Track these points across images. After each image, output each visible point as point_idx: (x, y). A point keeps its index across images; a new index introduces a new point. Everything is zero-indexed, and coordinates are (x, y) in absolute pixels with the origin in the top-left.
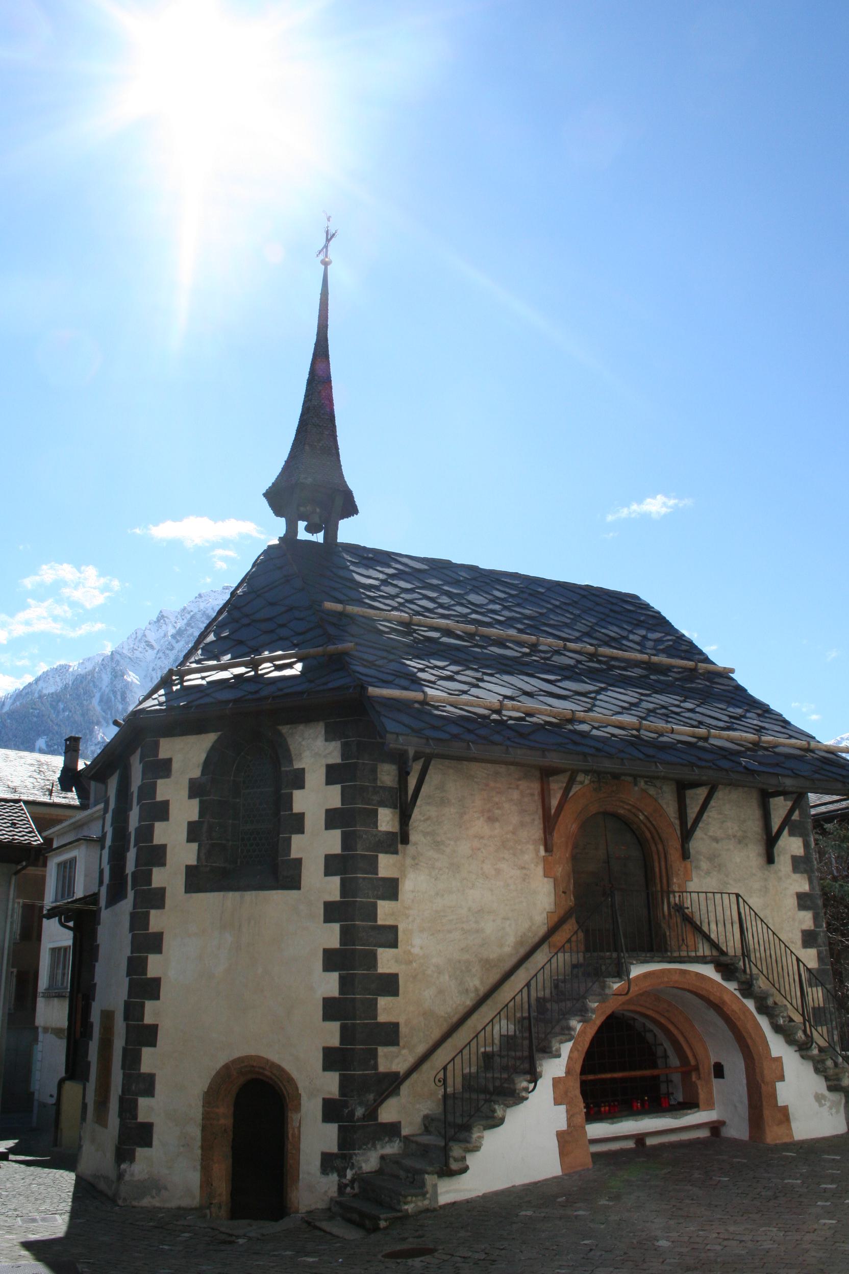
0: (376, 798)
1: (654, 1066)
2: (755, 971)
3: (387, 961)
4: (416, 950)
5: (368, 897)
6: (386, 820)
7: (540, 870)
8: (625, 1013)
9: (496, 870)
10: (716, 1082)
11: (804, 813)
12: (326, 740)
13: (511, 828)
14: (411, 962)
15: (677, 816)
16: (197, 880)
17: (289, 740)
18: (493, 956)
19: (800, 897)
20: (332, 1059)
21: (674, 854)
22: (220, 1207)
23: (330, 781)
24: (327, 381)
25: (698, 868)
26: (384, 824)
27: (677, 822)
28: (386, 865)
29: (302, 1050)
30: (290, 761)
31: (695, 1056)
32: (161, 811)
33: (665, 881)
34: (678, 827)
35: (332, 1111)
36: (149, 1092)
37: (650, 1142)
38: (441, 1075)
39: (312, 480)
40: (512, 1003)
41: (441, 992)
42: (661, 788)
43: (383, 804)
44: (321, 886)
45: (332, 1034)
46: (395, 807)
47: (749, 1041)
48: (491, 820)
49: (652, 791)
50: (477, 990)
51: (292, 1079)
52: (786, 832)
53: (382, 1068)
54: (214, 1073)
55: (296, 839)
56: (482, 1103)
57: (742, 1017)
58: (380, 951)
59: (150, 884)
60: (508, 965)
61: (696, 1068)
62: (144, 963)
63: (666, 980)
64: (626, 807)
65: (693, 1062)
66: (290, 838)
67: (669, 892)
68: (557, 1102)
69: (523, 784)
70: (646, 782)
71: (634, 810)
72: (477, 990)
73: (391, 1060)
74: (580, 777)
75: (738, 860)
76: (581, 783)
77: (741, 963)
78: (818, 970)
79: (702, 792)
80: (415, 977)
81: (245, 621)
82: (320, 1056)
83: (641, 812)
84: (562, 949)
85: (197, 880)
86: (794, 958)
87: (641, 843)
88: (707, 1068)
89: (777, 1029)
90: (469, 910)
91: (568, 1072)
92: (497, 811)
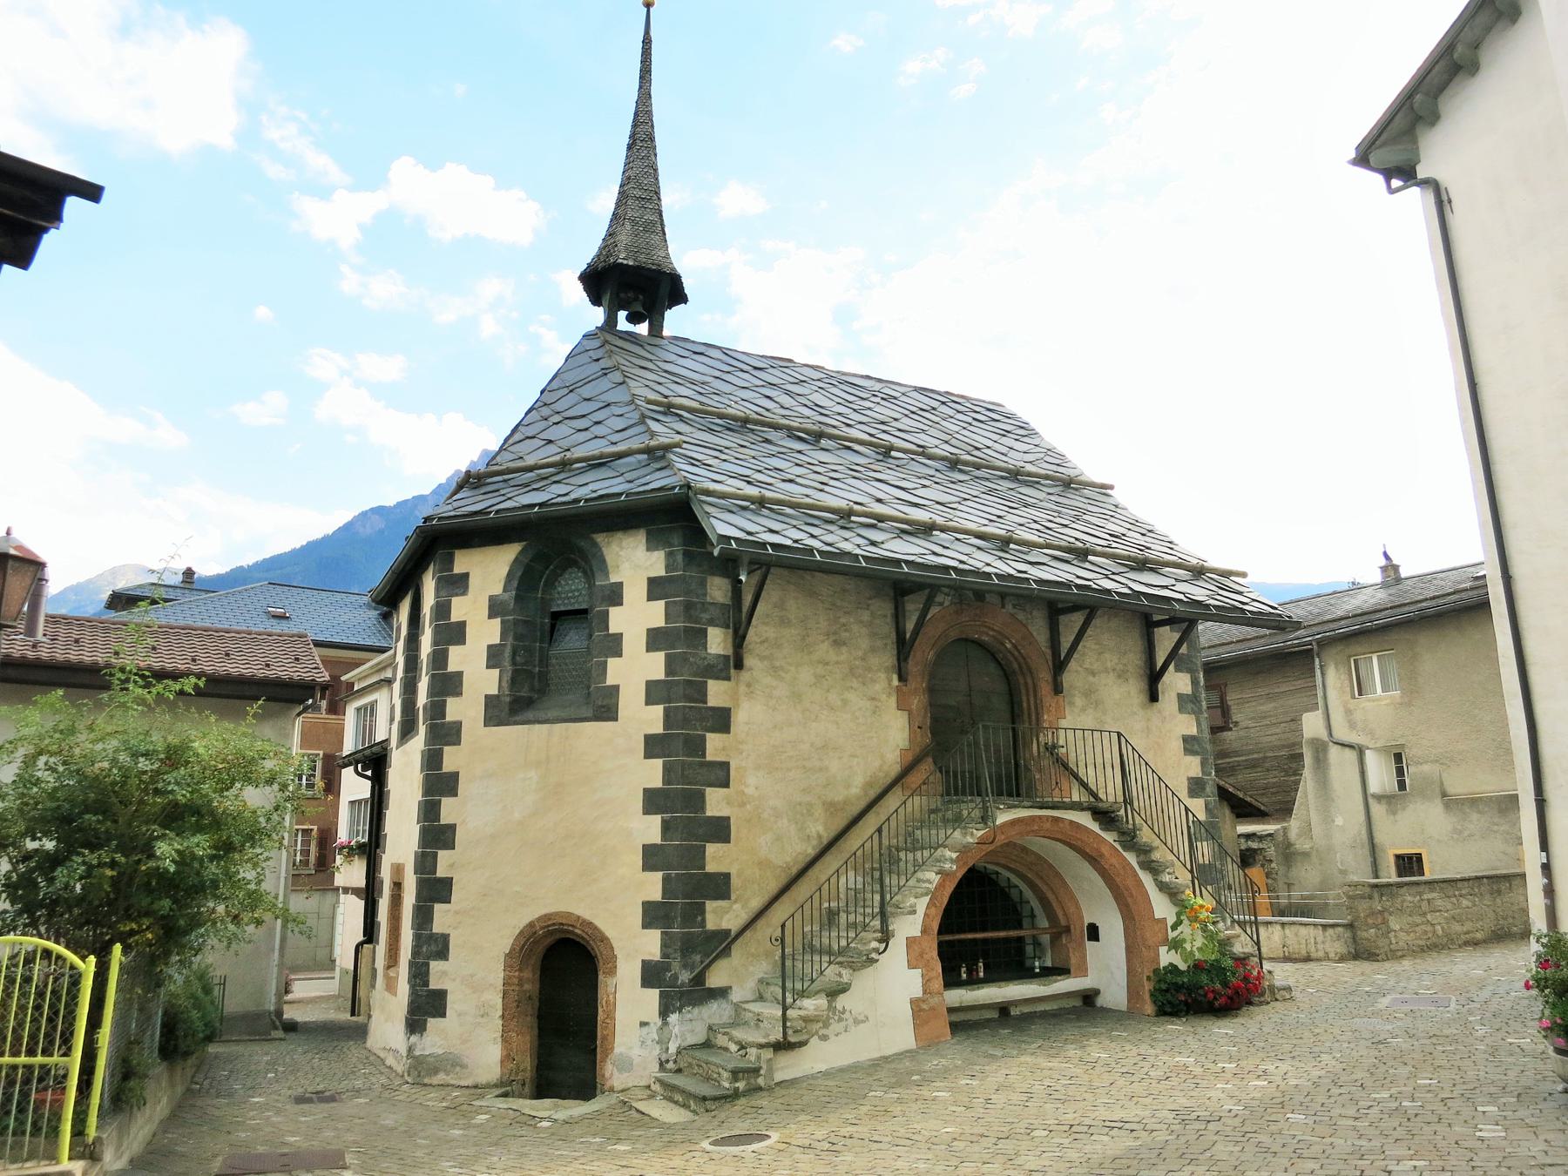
0: (705, 616)
1: (1019, 926)
2: (1138, 820)
3: (716, 803)
4: (750, 791)
6: (717, 642)
7: (893, 701)
8: (990, 867)
10: (1090, 945)
11: (1194, 646)
13: (860, 653)
16: (501, 711)
17: (605, 551)
18: (839, 798)
19: (1187, 740)
20: (653, 915)
21: (1045, 688)
23: (652, 596)
24: (649, 113)
25: (1072, 704)
27: (1049, 651)
28: (717, 693)
31: (1065, 914)
32: (452, 634)
34: (1049, 657)
35: (651, 975)
36: (443, 954)
38: (778, 933)
39: (633, 283)
40: (859, 853)
41: (778, 838)
43: (712, 623)
45: (652, 886)
46: (727, 627)
48: (838, 643)
49: (1021, 616)
50: (820, 837)
52: (1171, 667)
55: (612, 663)
56: (825, 965)
58: (709, 790)
59: (444, 717)
61: (1068, 930)
65: (1063, 923)
67: (1038, 727)
68: (911, 966)
70: (1014, 606)
72: (820, 837)
74: (939, 598)
75: (1117, 696)
76: (941, 604)
77: (1122, 812)
79: (1077, 619)
80: (749, 821)
81: (557, 418)
84: (916, 791)
85: (501, 711)
87: (1008, 676)
89: (1163, 887)
90: (812, 745)
91: (924, 931)
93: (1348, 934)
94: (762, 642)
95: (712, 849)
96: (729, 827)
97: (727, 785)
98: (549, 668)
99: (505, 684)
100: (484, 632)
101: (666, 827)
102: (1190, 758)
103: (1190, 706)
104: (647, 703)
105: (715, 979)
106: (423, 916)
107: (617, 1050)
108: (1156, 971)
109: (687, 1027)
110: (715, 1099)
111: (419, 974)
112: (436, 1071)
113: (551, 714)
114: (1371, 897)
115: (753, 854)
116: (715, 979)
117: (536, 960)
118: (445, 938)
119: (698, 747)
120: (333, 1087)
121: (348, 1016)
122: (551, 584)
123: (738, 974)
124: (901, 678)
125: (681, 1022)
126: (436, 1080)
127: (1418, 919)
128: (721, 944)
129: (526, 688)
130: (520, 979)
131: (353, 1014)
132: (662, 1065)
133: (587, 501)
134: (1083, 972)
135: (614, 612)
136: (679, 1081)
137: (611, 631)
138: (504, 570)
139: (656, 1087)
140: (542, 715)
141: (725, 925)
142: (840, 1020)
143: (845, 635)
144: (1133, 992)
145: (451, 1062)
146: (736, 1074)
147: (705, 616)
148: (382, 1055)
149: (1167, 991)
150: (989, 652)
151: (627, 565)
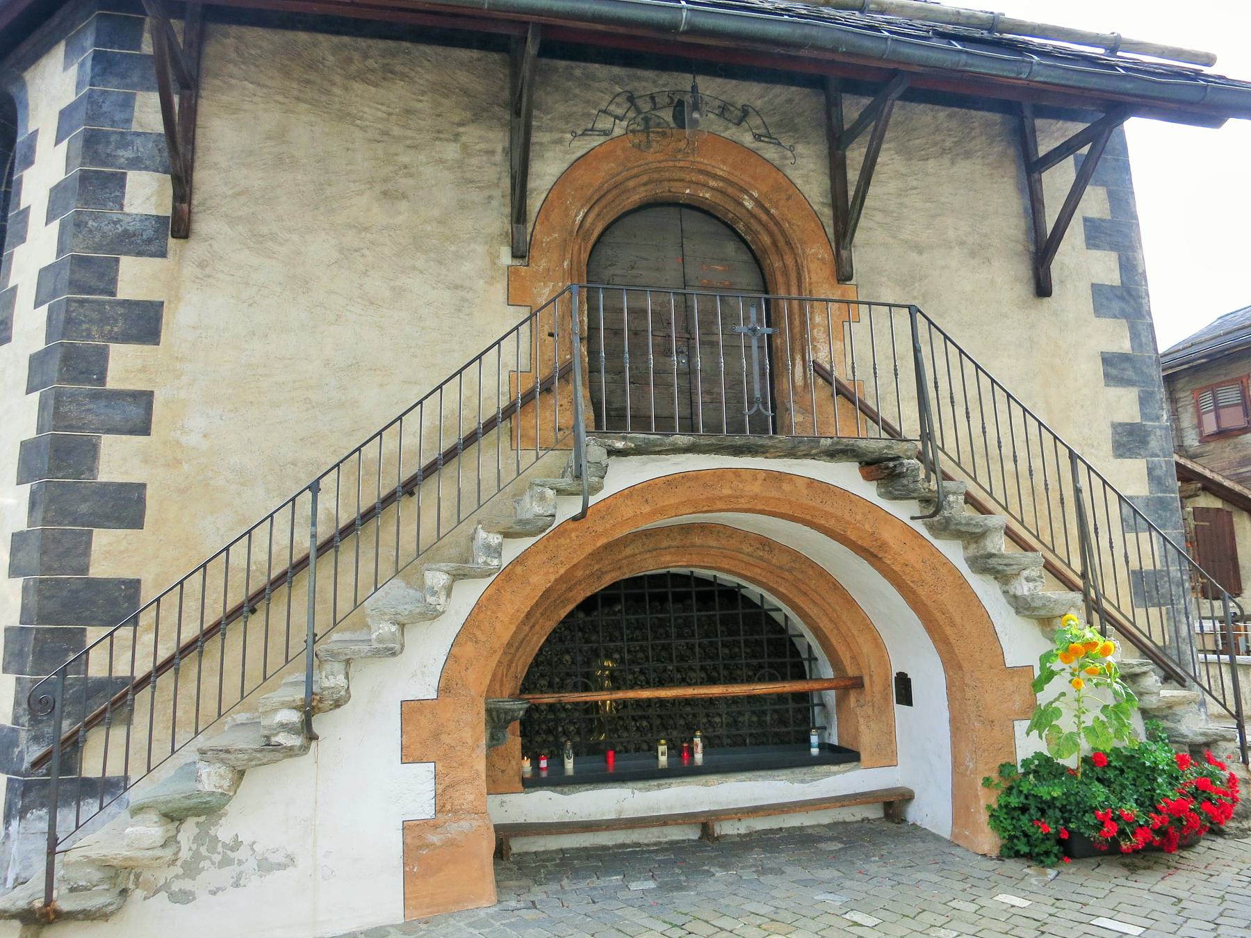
6: (145, 194)
7: (499, 291)
9: (394, 288)
10: (900, 710)
14: (178, 462)
15: (829, 200)
27: (827, 212)
28: (135, 278)
33: (797, 322)
42: (792, 148)
43: (136, 164)
49: (770, 153)
57: (929, 578)
63: (726, 491)
64: (712, 183)
68: (407, 756)
69: (472, 134)
71: (730, 190)
78: (1148, 502)
83: (746, 192)
86: (1063, 452)
87: (757, 261)
88: (879, 686)
90: (327, 363)
91: (445, 688)
92: (404, 181)
93: (1180, 384)
95: (103, 539)
96: (141, 501)
97: (145, 430)
102: (1116, 392)
103: (1116, 305)
128: (116, 700)
134: (888, 756)
142: (226, 862)
143: (404, 183)
147: (128, 154)
149: (1024, 809)
150: (718, 220)
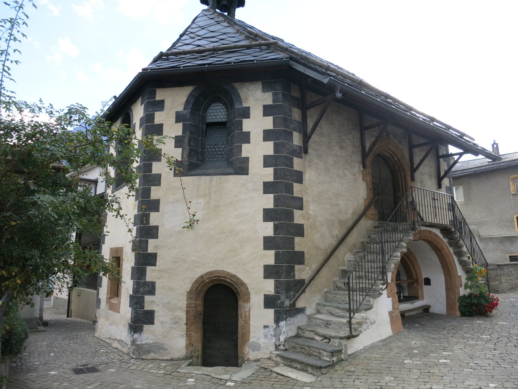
0: (292, 126)
3: (298, 217)
4: (311, 212)
5: (289, 180)
6: (297, 139)
12: (263, 92)
17: (239, 91)
20: (269, 272)
21: (409, 179)
22: (198, 358)
23: (265, 114)
26: (296, 141)
27: (409, 163)
28: (297, 164)
29: (251, 267)
30: (241, 103)
31: (416, 274)
35: (269, 302)
37: (406, 315)
43: (294, 129)
44: (261, 173)
45: (269, 258)
46: (301, 133)
47: (450, 268)
48: (342, 148)
50: (337, 236)
51: (245, 284)
53: (297, 277)
54: (194, 280)
55: (245, 146)
59: (151, 172)
60: (350, 224)
61: (417, 281)
62: (148, 217)
65: (415, 277)
66: (241, 146)
72: (337, 236)
73: (302, 273)
82: (262, 270)
94: (314, 142)
98: (210, 147)
99: (185, 156)
100: (173, 129)
101: (276, 228)
104: (264, 166)
105: (300, 304)
106: (139, 272)
107: (251, 340)
108: (459, 298)
109: (288, 328)
110: (326, 367)
111: (137, 301)
112: (149, 352)
113: (210, 171)
114: (497, 270)
115: (313, 243)
116: (300, 304)
117: (202, 295)
118: (153, 284)
119: (290, 189)
120: (95, 361)
121: (64, 316)
122: (206, 109)
123: (308, 301)
124: (364, 167)
125: (286, 325)
126: (149, 357)
127: (508, 278)
128: (300, 286)
129: (195, 158)
130: (196, 304)
131: (68, 317)
132: (277, 347)
133: (234, 63)
134: (423, 299)
135: (245, 121)
136: (286, 354)
137: (243, 131)
138: (185, 99)
139: (279, 359)
140: (205, 171)
141: (303, 277)
144: (449, 306)
145: (158, 347)
146: (332, 353)
148: (108, 341)
151: (252, 98)
